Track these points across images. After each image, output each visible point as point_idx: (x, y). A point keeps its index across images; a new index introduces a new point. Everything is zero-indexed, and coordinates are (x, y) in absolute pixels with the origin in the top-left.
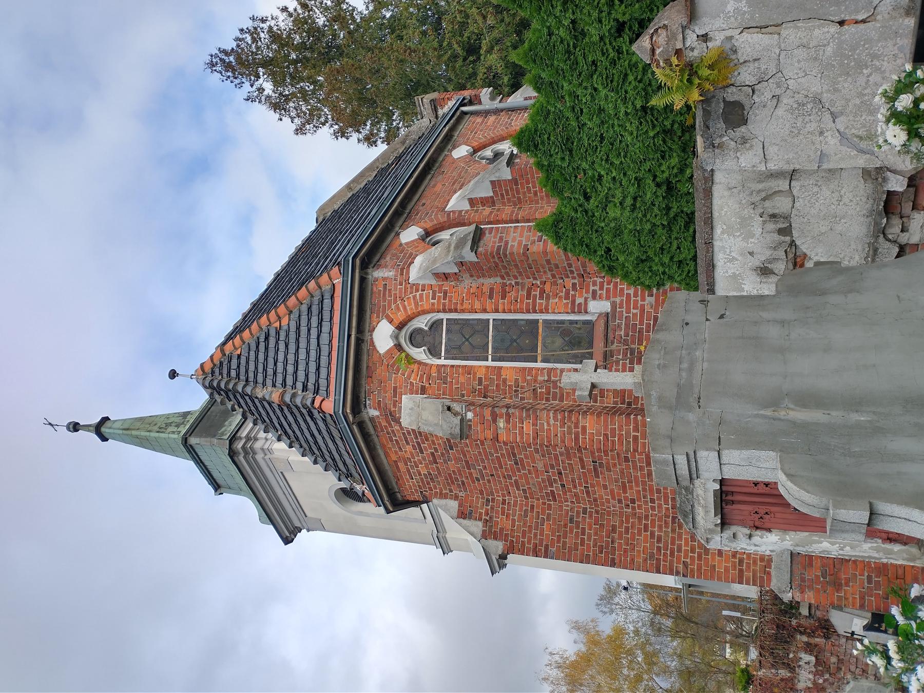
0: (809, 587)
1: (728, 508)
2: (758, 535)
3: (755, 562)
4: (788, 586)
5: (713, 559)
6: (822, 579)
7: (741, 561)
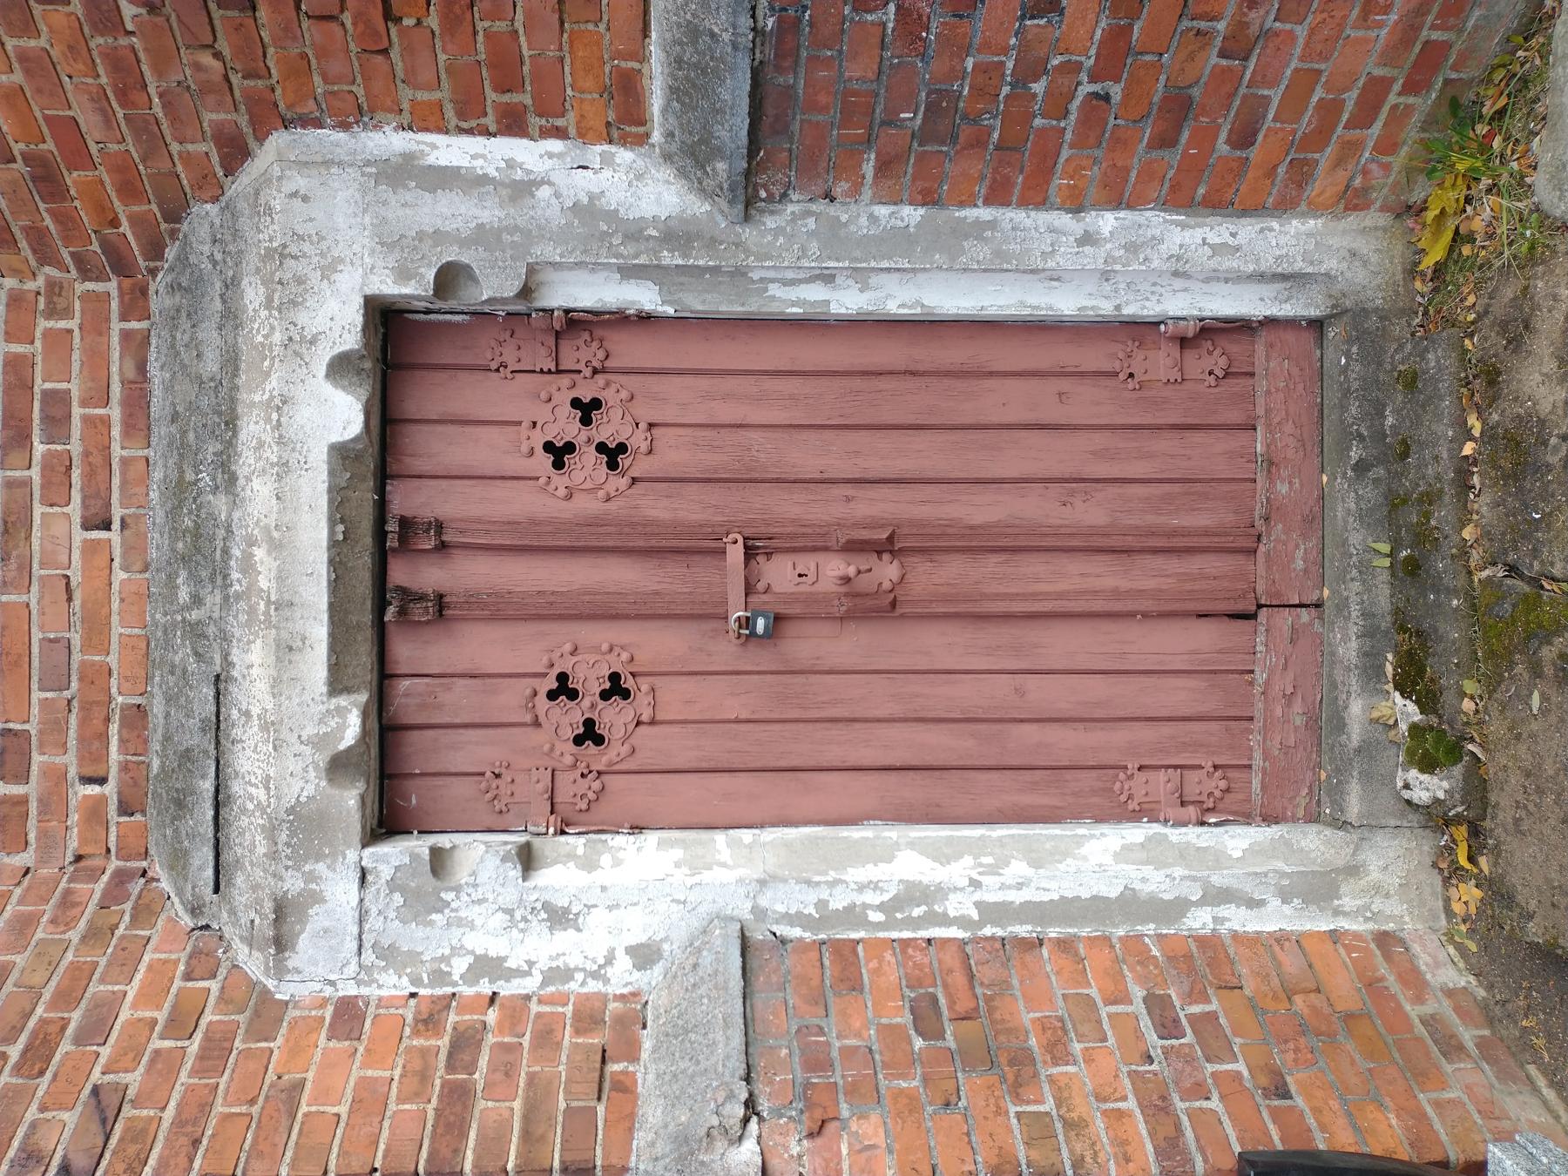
0: (852, 1091)
1: (406, 651)
2: (571, 856)
3: (546, 1037)
4: (731, 1096)
5: (296, 1050)
6: (919, 1043)
7: (465, 1045)
